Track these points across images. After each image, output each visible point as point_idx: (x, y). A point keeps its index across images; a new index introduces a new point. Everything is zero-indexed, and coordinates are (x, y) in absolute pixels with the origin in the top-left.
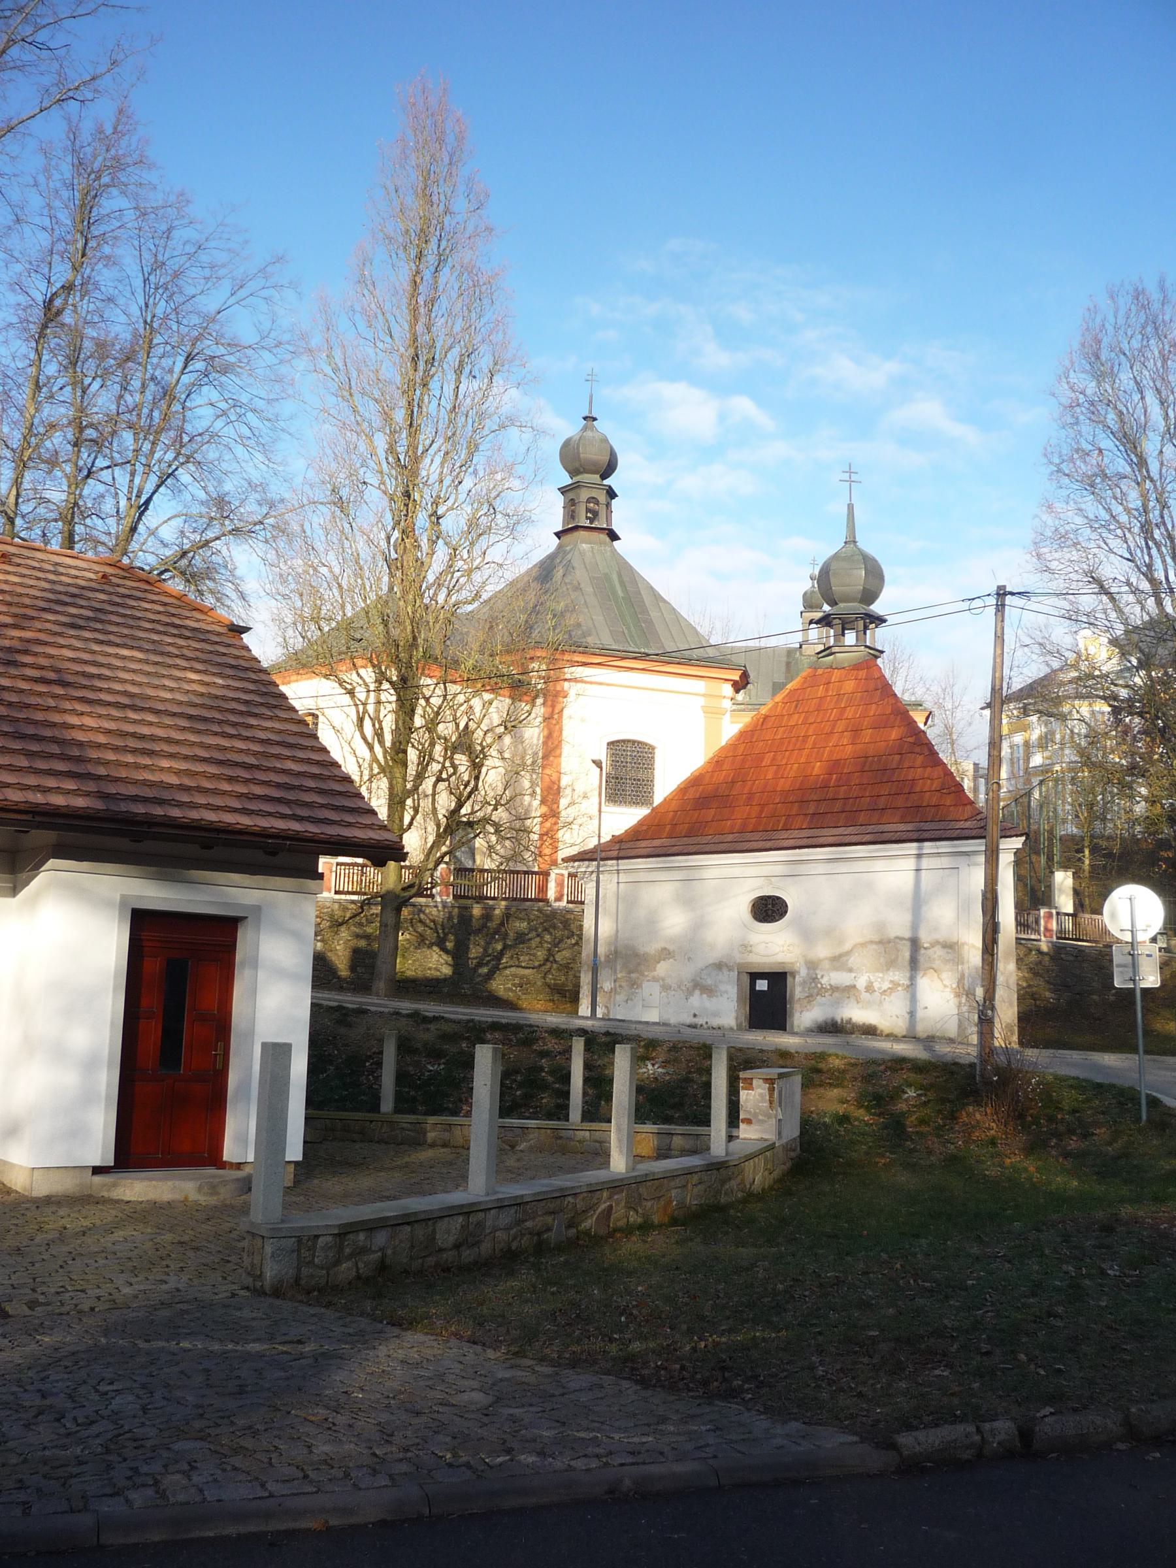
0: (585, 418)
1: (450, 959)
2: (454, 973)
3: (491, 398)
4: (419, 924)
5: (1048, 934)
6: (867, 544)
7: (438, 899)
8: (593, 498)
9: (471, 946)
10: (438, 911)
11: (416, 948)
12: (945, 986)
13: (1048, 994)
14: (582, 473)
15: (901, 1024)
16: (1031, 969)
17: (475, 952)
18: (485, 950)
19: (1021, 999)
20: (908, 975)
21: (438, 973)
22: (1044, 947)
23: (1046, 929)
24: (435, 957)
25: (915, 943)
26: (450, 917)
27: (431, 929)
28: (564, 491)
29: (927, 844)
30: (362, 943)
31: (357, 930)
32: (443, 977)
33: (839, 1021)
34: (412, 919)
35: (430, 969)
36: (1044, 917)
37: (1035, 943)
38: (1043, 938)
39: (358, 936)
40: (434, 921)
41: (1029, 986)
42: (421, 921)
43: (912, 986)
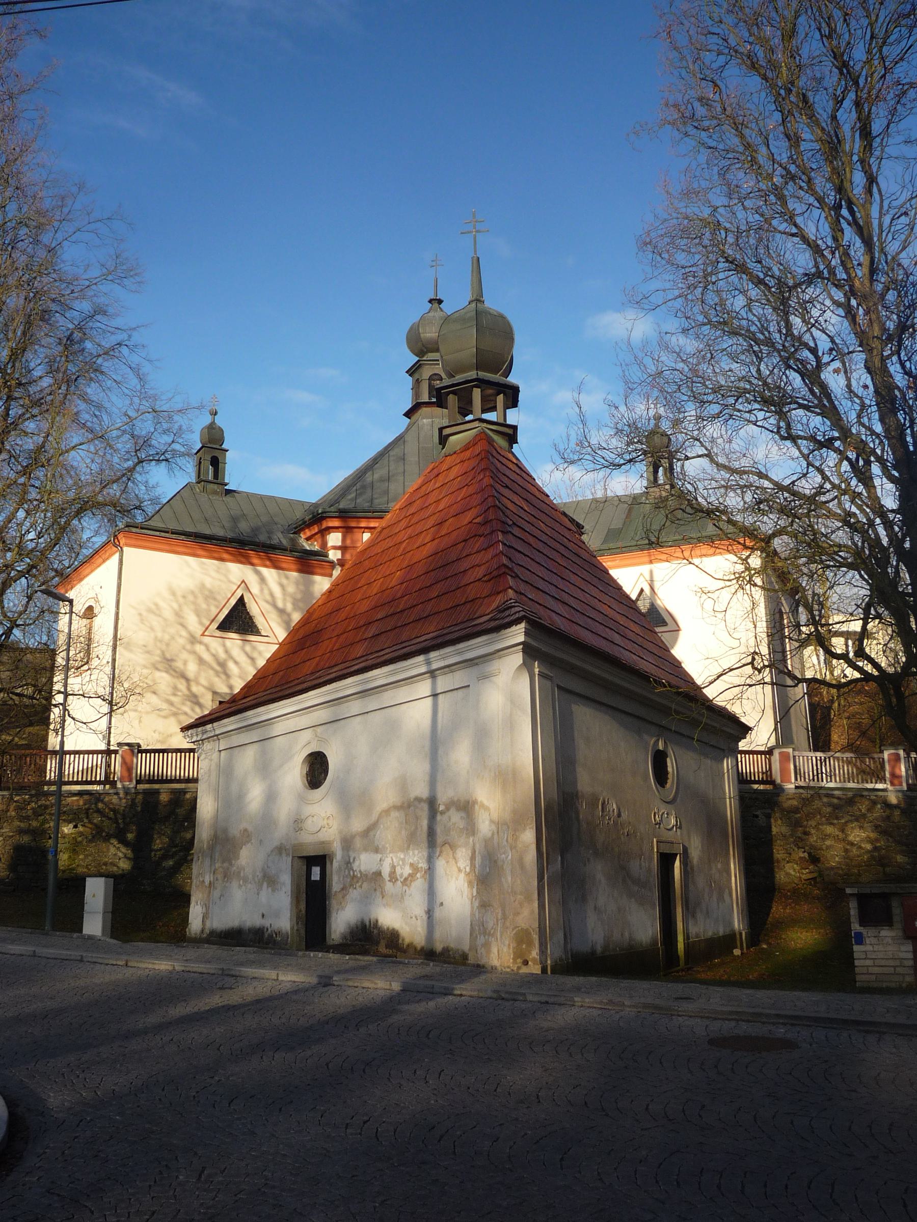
0: (431, 301)
1: (129, 853)
2: (133, 868)
4: (95, 815)
5: (896, 782)
6: (491, 303)
7: (119, 785)
8: (435, 374)
9: (155, 836)
10: (120, 799)
11: (91, 841)
12: (460, 870)
13: (900, 858)
14: (426, 353)
15: (419, 929)
16: (877, 827)
17: (159, 843)
18: (172, 840)
20: (425, 854)
21: (115, 869)
22: (893, 799)
23: (894, 776)
24: (112, 850)
25: (432, 802)
26: (133, 803)
27: (110, 819)
28: (411, 372)
29: (433, 655)
30: (26, 839)
31: (22, 825)
32: (120, 872)
33: (368, 924)
34: (88, 809)
35: (105, 864)
36: (889, 761)
37: (880, 793)
38: (890, 787)
39: (21, 832)
40: (114, 811)
41: (876, 849)
42: (98, 811)
43: (430, 871)
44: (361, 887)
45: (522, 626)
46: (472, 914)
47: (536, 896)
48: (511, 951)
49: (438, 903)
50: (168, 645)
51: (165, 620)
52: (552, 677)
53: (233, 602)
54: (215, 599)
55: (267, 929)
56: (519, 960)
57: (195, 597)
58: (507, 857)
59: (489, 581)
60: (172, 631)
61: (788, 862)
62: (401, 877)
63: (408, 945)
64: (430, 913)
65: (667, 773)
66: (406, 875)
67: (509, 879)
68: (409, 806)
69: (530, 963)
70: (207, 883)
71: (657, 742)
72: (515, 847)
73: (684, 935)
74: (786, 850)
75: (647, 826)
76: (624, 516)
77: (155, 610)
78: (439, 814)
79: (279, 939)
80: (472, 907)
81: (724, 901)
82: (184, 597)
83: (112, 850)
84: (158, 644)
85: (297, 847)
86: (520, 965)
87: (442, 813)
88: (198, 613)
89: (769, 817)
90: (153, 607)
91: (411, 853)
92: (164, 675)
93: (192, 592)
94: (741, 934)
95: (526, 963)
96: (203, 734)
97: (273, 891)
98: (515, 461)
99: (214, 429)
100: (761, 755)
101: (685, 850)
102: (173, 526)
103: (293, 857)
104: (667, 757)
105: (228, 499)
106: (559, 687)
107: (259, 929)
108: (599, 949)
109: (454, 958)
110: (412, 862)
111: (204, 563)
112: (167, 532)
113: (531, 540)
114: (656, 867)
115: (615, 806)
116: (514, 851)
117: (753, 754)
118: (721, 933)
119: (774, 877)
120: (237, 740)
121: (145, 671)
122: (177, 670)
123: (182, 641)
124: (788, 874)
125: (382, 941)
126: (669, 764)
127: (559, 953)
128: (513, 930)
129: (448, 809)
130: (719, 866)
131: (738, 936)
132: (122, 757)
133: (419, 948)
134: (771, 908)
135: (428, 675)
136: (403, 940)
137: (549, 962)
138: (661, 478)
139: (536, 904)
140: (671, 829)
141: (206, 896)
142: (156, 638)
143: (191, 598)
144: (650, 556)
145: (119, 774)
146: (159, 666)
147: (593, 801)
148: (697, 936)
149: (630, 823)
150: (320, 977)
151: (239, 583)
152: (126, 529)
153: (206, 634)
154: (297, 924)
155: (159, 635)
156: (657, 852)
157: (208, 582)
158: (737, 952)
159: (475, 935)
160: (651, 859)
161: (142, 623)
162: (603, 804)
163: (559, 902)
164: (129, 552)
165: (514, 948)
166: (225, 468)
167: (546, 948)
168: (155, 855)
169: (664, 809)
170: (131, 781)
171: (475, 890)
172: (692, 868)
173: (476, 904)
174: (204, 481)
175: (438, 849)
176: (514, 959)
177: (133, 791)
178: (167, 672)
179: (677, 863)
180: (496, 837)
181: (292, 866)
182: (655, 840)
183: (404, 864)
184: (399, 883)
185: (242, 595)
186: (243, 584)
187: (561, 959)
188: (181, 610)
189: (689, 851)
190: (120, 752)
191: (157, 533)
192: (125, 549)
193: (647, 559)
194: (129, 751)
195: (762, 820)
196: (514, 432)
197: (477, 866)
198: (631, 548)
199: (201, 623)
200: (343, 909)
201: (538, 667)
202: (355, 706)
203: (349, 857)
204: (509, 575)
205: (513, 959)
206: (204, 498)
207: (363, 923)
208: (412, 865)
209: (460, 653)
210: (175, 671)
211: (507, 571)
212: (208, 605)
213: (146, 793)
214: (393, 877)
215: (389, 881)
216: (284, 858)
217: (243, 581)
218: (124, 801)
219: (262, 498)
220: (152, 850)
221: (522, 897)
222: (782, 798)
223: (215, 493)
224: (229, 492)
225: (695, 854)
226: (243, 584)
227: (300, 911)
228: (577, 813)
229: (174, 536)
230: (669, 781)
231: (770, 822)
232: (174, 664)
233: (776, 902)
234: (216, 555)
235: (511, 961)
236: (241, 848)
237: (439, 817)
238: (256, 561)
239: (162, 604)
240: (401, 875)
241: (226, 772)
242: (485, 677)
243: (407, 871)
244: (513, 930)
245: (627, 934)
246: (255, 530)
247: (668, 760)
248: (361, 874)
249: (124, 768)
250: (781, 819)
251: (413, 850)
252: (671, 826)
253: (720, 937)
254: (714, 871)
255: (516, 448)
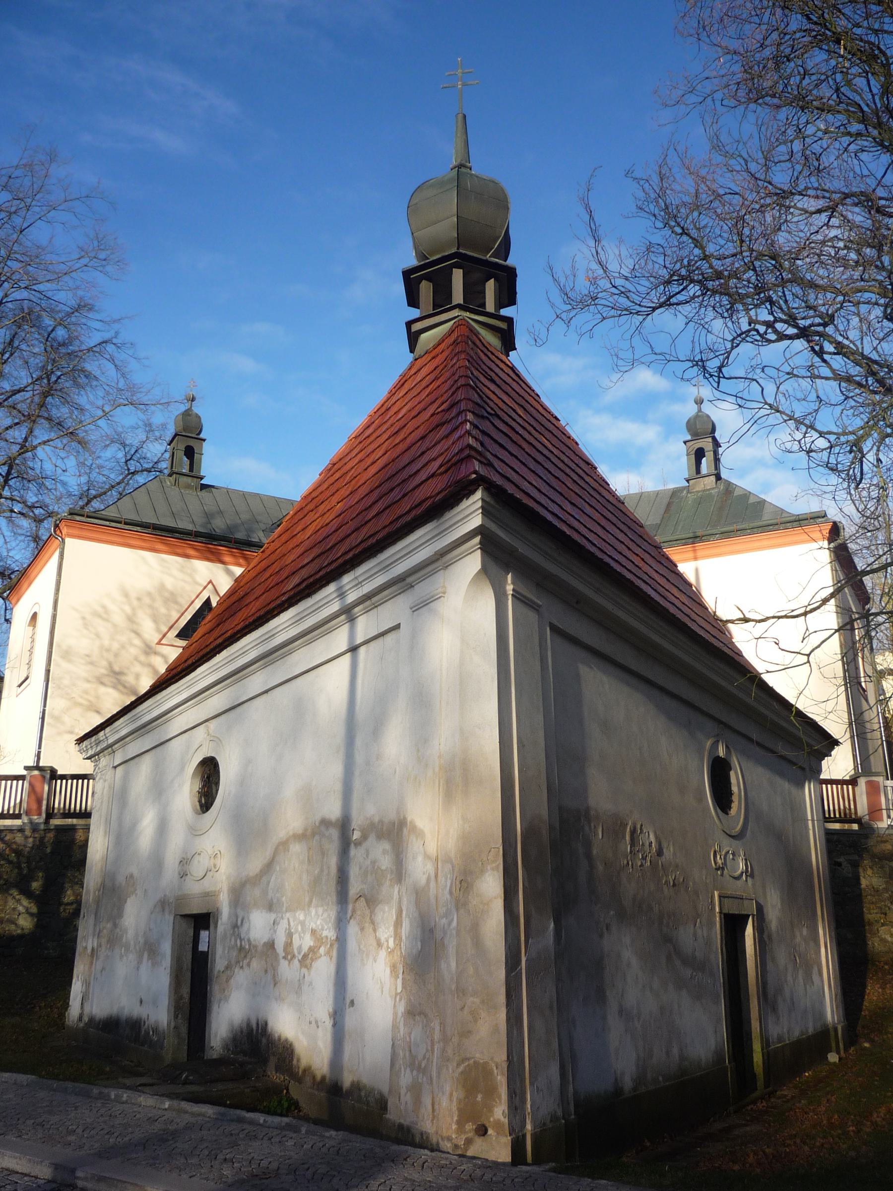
2: (37, 926)
3: (714, 217)
6: (480, 167)
9: (67, 885)
10: (26, 837)
19: (175, 423)
20: (333, 914)
21: (13, 927)
25: (344, 825)
32: (19, 931)
33: (254, 1026)
40: (18, 853)
43: (341, 940)
44: (249, 965)
45: (477, 498)
46: (395, 1027)
47: (502, 998)
48: (454, 1109)
49: (348, 1001)
50: (116, 655)
51: (115, 626)
52: (539, 606)
53: (198, 605)
54: (176, 603)
55: (145, 1022)
56: (470, 1126)
57: (153, 599)
58: (450, 924)
59: (446, 471)
60: (123, 639)
61: (883, 925)
62: (299, 953)
63: (305, 1071)
64: (337, 1016)
65: (730, 794)
66: (305, 949)
67: (453, 965)
68: (314, 834)
69: (490, 1132)
70: (89, 950)
71: (715, 746)
72: (465, 904)
73: (762, 1043)
74: (880, 908)
75: (704, 872)
76: (662, 511)
77: (103, 614)
78: (352, 845)
79: (155, 1038)
80: (395, 1014)
81: (813, 982)
82: (139, 599)
83: (11, 903)
84: (105, 654)
85: (181, 899)
86: (470, 1135)
87: (358, 844)
88: (155, 619)
89: (855, 865)
90: (100, 610)
91: (313, 911)
92: (111, 691)
93: (149, 594)
94: (836, 1029)
95: (482, 1131)
96: (97, 744)
97: (153, 965)
98: (510, 365)
99: (189, 415)
100: (842, 785)
101: (760, 908)
102: (133, 517)
103: (176, 915)
104: (731, 769)
105: (204, 494)
106: (554, 629)
107: (136, 1022)
108: (628, 1083)
109: (368, 1104)
110: (314, 926)
111: (163, 560)
112: (120, 522)
113: (525, 445)
114: (719, 937)
115: (652, 838)
116: (462, 911)
117: (837, 784)
118: (811, 1031)
119: (865, 944)
120: (134, 748)
121: (87, 686)
122: (127, 685)
123: (133, 651)
124: (883, 941)
125: (272, 1058)
126: (733, 780)
127: (550, 1105)
128: (458, 1065)
129: (365, 837)
130: (805, 931)
131: (832, 1033)
132: (31, 784)
133: (319, 1078)
134: (864, 986)
135: (343, 617)
136: (298, 1060)
137: (529, 1127)
138: (704, 469)
139: (502, 1015)
140: (738, 878)
141: (87, 968)
142: (102, 647)
143: (147, 600)
144: (695, 551)
145: (26, 806)
146: (105, 680)
147: (616, 827)
148: (780, 1039)
149: (677, 866)
150: (56, 1167)
151: (205, 584)
152: (69, 517)
153: (163, 642)
154: (176, 1017)
155: (106, 643)
156: (720, 913)
157: (169, 583)
158: (833, 1058)
159: (397, 1066)
160: (711, 924)
161: (88, 629)
162: (633, 832)
163: (551, 1008)
164: (73, 545)
165: (459, 1101)
166: (201, 459)
167: (523, 1101)
168: (65, 910)
169: (728, 845)
170: (40, 814)
171: (399, 982)
172: (770, 937)
173: (401, 1009)
174: (177, 473)
175: (350, 907)
176: (460, 1123)
177: (42, 827)
178: (114, 687)
179: (749, 930)
180: (433, 884)
181: (173, 929)
182: (716, 894)
183: (304, 931)
184: (296, 962)
185: (209, 597)
186: (210, 586)
187: (554, 1118)
188: (134, 614)
189: (765, 911)
190: (28, 778)
191: (107, 523)
192: (68, 540)
193: (691, 555)
194: (40, 778)
195: (846, 869)
196: (508, 326)
197: (404, 938)
198: (670, 543)
199: (158, 630)
200: (226, 999)
201: (513, 583)
202: (257, 682)
203: (237, 917)
204: (476, 459)
205: (458, 1122)
206: (174, 493)
207: (249, 1024)
208: (313, 932)
209: (386, 568)
210: (125, 687)
211: (473, 453)
212: (168, 609)
213: (60, 829)
214: (289, 954)
215: (285, 958)
216: (167, 916)
217: (210, 582)
218: (31, 840)
219: (244, 495)
220: (61, 904)
221: (477, 1000)
222: (871, 842)
223: (188, 487)
224: (204, 487)
225: (774, 913)
226: (210, 586)
227: (181, 998)
228: (588, 845)
229: (127, 527)
230: (735, 806)
231: (858, 872)
232: (123, 678)
233: (871, 979)
234: (179, 551)
235: (454, 1127)
236: (126, 902)
237: (353, 852)
238: (227, 559)
239: (112, 607)
240: (300, 948)
241: (121, 796)
242: (422, 605)
243: (308, 942)
244: (458, 1065)
245: (675, 1051)
246: (232, 528)
247: (732, 773)
248: (250, 945)
249: (33, 797)
250: (871, 868)
251: (317, 906)
252: (739, 872)
253: (809, 1038)
254: (798, 939)
255: (513, 357)
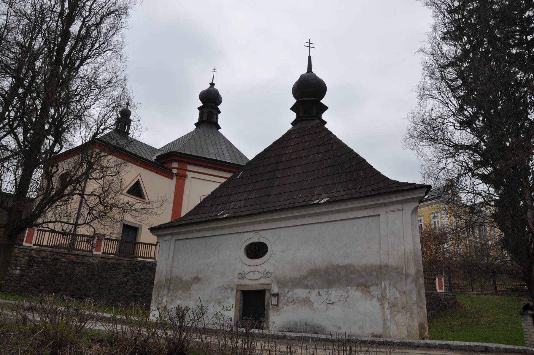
6: (317, 71)
185: (139, 180)
217: (140, 174)
